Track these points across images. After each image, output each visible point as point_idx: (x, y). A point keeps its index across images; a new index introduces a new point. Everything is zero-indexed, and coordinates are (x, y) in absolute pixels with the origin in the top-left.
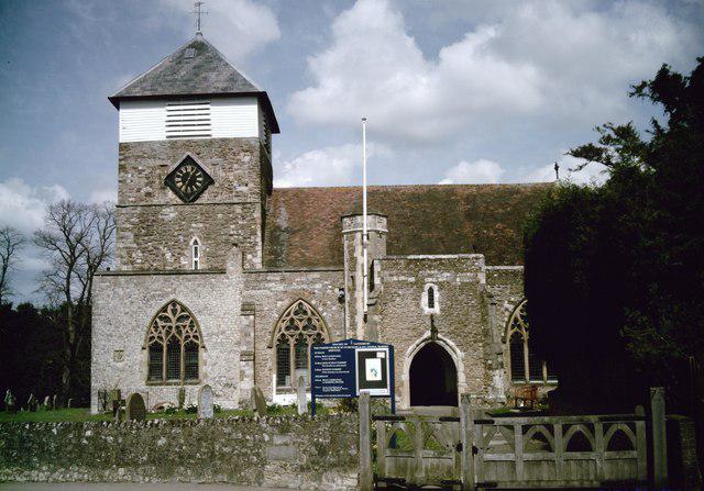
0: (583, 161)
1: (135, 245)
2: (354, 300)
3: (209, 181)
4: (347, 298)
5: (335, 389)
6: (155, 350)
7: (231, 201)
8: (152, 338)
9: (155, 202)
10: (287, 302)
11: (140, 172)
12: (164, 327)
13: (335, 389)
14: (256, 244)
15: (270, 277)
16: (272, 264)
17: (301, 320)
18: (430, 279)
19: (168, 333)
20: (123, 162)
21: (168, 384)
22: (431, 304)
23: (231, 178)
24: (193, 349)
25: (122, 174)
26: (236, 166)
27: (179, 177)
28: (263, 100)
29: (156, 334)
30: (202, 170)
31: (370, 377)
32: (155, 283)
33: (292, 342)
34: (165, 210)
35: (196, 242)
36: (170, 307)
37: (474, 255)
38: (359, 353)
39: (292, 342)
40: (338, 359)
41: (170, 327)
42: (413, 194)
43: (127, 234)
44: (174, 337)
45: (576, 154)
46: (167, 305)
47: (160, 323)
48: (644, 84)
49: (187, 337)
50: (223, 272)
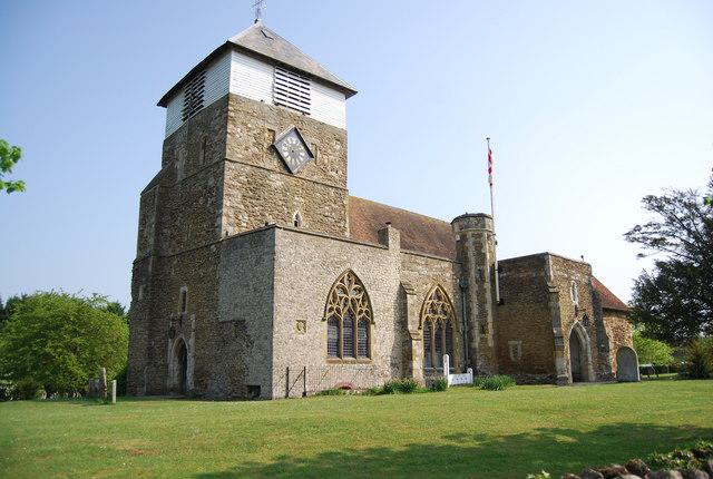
8: (331, 309)
9: (262, 165)
10: (429, 286)
11: (249, 130)
12: (341, 298)
19: (345, 305)
49: (361, 312)
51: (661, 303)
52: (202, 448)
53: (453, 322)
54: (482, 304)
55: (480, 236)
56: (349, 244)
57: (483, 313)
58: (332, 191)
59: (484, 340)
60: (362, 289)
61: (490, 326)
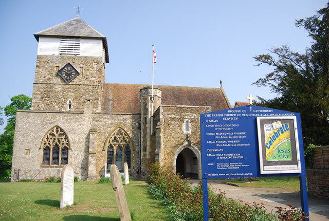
2: (145, 129)
4: (142, 127)
5: (232, 166)
6: (47, 149)
9: (52, 82)
10: (113, 129)
11: (46, 69)
12: (51, 139)
13: (232, 166)
14: (98, 103)
15: (105, 116)
16: (105, 112)
18: (187, 117)
19: (54, 142)
20: (38, 64)
22: (187, 129)
23: (88, 74)
24: (66, 150)
25: (38, 69)
28: (104, 40)
31: (270, 159)
32: (48, 117)
34: (56, 86)
36: (55, 129)
37: (207, 107)
38: (261, 120)
40: (235, 130)
41: (55, 139)
42: (165, 89)
43: (38, 96)
44: (56, 144)
45: (258, 59)
46: (54, 127)
47: (50, 137)
48: (302, 21)
49: (63, 144)
50: (82, 113)
51: (204, 190)
53: (130, 145)
55: (146, 99)
56: (38, 115)
58: (91, 88)
59: (145, 155)
61: (148, 148)
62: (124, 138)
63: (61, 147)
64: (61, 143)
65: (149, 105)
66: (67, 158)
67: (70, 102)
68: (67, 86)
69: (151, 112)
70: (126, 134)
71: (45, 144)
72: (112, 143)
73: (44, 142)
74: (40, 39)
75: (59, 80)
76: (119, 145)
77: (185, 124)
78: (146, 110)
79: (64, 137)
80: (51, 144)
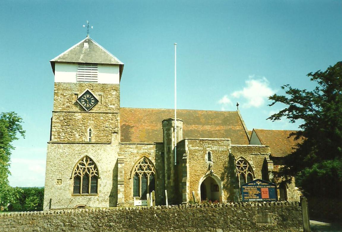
0: (274, 101)
1: (61, 130)
3: (97, 101)
6: (77, 178)
7: (106, 112)
9: (71, 110)
11: (65, 96)
12: (81, 168)
17: (144, 166)
19: (84, 171)
20: (56, 91)
21: (83, 196)
22: (209, 159)
23: (107, 101)
25: (56, 97)
26: (109, 96)
27: (89, 96)
29: (77, 172)
30: (94, 97)
32: (77, 147)
33: (141, 176)
35: (90, 130)
36: (85, 158)
39: (141, 176)
41: (85, 168)
47: (80, 166)
49: (93, 173)
52: (80, 207)
54: (169, 163)
56: (68, 145)
57: (169, 169)
59: (169, 183)
60: (93, 163)
61: (172, 175)
62: (148, 166)
63: (90, 176)
64: (91, 172)
65: (173, 136)
66: (97, 186)
67: (90, 130)
68: (87, 114)
69: (174, 142)
70: (151, 162)
71: (75, 173)
72: (138, 172)
73: (74, 172)
74: (57, 66)
75: (77, 109)
76: (144, 173)
77: (207, 155)
78: (169, 141)
79: (93, 166)
80: (81, 173)
